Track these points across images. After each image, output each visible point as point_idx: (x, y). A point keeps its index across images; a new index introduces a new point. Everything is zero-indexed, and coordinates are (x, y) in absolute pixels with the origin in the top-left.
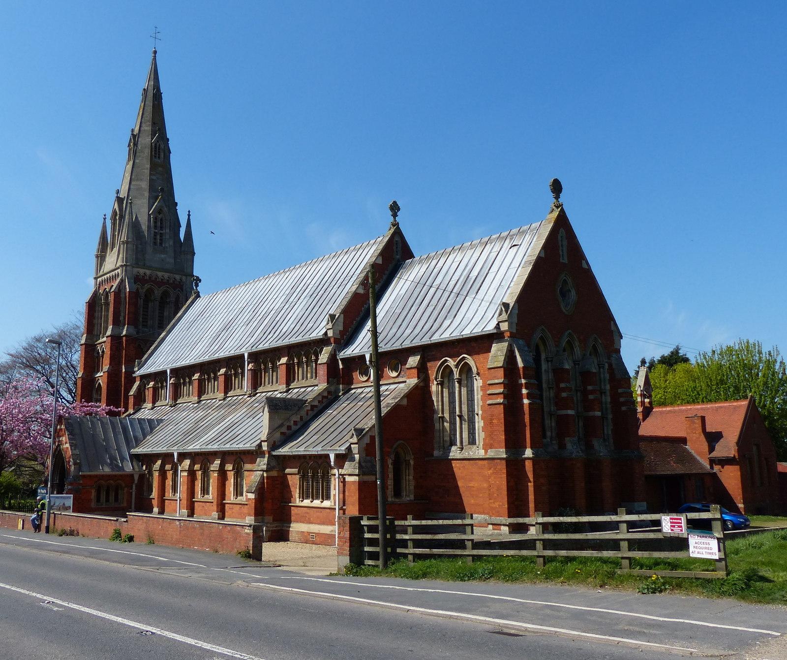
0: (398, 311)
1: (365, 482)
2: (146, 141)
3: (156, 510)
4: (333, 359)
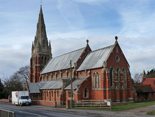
0: (87, 62)
1: (79, 94)
2: (40, 25)
3: (44, 100)
4: (75, 71)
